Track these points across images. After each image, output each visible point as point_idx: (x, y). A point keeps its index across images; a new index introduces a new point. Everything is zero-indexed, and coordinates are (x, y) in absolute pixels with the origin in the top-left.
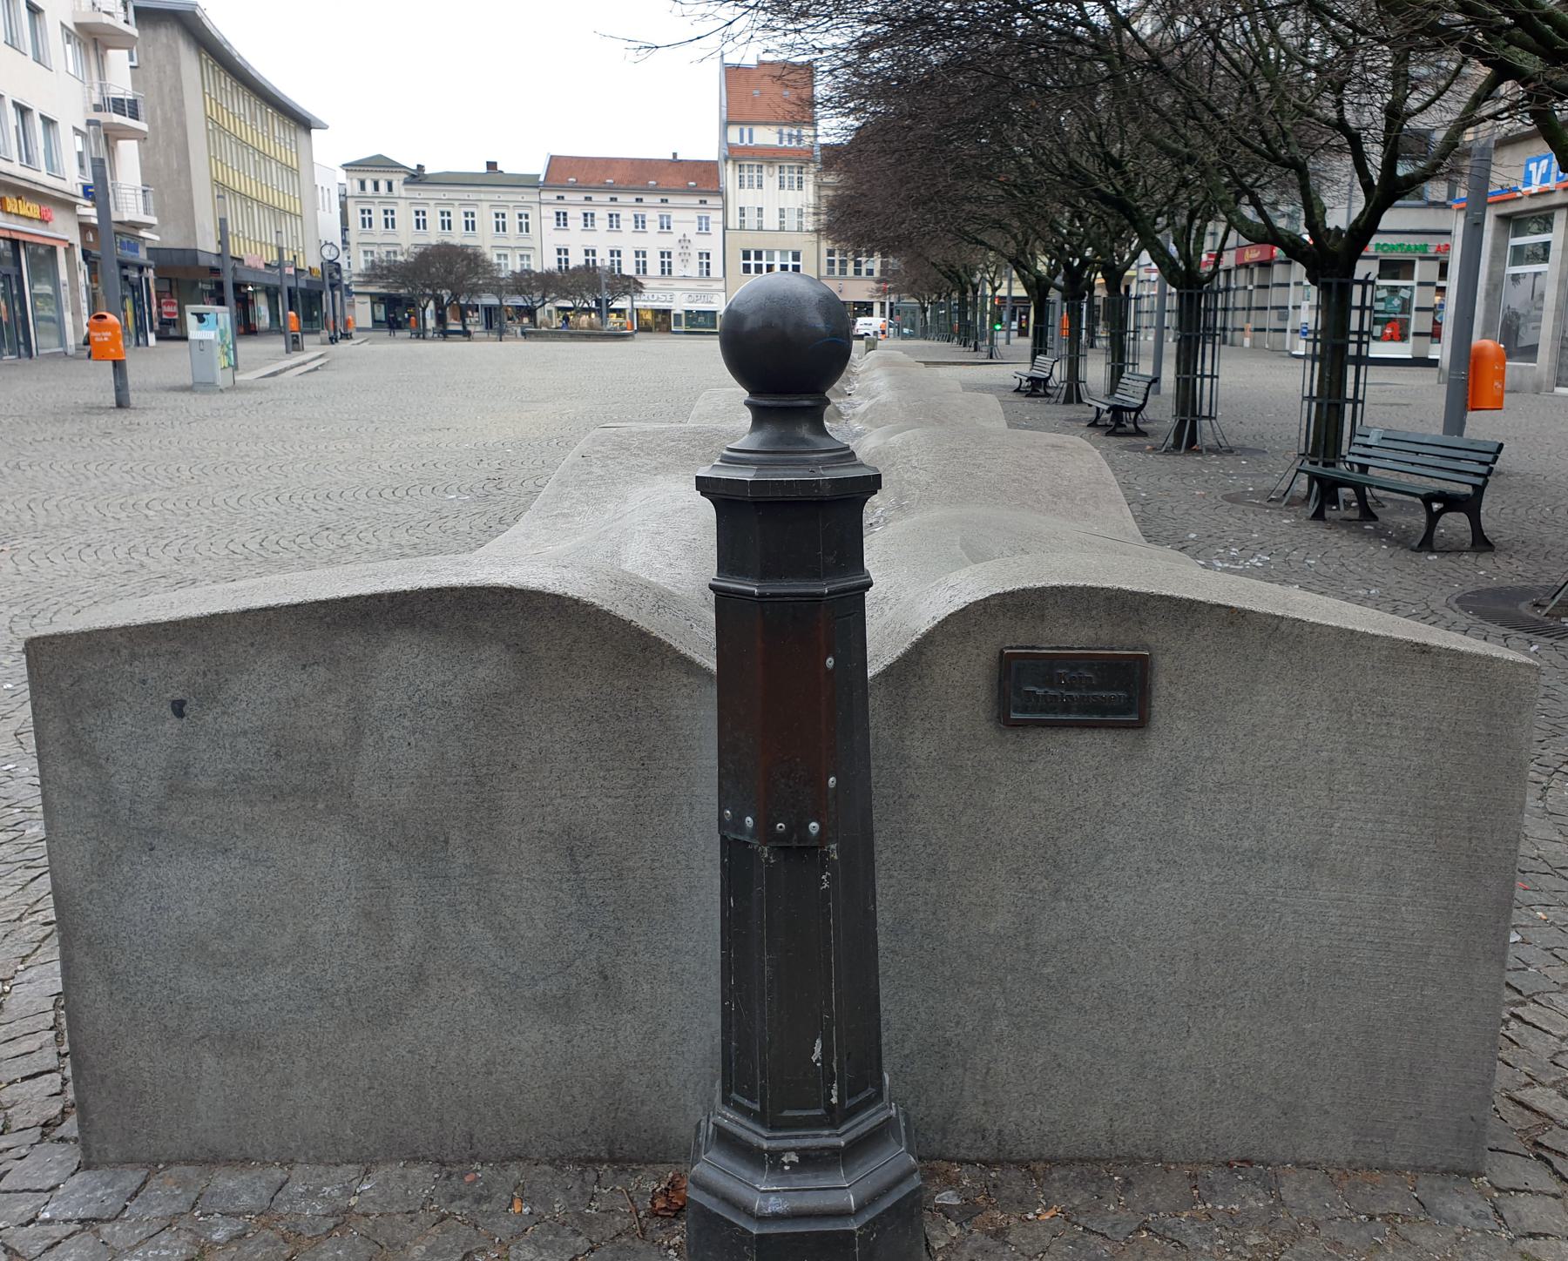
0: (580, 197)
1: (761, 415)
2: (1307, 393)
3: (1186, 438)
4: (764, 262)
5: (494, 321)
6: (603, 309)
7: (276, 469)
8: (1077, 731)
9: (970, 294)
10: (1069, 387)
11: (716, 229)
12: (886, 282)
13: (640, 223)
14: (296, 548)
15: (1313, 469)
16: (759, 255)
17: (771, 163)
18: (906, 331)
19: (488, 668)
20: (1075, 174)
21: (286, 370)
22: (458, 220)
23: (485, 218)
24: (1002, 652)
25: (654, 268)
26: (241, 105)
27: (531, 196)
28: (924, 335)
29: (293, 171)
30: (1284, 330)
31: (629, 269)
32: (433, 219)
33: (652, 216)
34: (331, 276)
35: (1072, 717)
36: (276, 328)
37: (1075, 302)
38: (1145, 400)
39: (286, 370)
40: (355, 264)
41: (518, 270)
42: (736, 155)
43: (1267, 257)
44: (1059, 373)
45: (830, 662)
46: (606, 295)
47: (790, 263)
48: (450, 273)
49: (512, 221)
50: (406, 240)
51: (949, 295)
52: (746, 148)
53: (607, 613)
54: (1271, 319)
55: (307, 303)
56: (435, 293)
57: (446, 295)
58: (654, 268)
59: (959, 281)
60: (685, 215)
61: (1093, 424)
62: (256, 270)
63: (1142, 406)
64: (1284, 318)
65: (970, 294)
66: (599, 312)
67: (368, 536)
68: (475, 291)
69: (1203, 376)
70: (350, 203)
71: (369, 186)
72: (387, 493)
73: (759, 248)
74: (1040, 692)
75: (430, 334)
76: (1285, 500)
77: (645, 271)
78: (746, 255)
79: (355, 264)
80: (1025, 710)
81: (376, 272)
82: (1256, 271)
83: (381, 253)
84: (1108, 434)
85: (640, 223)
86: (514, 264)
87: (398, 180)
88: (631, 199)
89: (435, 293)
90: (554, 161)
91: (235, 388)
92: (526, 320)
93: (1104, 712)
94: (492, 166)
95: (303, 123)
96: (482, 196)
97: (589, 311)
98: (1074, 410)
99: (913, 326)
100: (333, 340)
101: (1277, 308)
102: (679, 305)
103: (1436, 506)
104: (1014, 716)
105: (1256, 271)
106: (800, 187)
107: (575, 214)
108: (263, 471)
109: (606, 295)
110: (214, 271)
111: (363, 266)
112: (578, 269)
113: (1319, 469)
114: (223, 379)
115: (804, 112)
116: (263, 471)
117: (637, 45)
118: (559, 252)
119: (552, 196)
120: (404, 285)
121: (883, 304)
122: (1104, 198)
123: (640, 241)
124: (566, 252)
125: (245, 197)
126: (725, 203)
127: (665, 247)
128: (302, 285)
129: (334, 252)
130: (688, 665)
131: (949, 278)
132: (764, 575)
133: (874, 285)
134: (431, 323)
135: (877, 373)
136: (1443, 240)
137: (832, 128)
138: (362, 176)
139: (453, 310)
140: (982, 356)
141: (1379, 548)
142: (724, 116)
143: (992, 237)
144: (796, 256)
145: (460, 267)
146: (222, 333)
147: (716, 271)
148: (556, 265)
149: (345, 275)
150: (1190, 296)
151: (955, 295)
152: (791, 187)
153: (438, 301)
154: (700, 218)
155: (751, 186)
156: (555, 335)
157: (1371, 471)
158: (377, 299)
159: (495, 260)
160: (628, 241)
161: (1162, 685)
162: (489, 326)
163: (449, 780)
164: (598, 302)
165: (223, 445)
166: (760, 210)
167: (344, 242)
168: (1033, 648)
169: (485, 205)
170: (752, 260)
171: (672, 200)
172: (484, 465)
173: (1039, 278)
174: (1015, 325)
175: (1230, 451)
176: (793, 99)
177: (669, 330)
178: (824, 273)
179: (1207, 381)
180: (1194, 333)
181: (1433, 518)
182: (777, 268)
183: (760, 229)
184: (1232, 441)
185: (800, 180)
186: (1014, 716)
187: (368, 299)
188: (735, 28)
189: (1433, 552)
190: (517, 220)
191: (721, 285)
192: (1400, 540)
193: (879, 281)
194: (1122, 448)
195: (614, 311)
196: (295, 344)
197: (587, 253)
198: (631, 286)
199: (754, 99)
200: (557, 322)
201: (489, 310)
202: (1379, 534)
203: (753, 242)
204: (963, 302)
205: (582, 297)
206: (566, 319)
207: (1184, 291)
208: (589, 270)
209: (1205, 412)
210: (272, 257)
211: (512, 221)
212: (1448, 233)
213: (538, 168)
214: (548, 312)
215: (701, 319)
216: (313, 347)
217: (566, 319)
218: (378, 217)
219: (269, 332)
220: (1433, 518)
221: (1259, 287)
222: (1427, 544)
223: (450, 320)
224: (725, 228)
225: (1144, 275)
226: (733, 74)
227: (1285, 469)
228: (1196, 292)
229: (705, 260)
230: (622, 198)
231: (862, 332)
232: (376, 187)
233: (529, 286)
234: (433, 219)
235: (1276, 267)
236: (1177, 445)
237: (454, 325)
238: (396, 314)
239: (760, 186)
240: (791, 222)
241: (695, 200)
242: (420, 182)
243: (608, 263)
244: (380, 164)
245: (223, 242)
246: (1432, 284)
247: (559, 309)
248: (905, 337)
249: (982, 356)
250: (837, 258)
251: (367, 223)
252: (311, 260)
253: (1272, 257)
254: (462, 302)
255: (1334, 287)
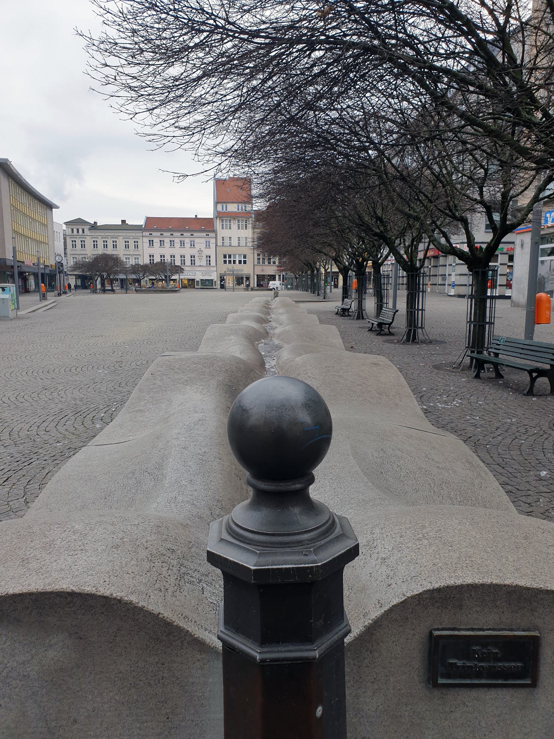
0: (158, 234)
1: (262, 498)
2: (469, 320)
3: (412, 335)
4: (232, 259)
5: (124, 284)
6: (167, 279)
7: (28, 358)
8: (486, 689)
9: (315, 272)
10: (359, 313)
11: (213, 246)
12: (281, 267)
13: (182, 244)
14: (31, 400)
15: (472, 355)
16: (230, 256)
17: (234, 219)
18: (289, 286)
19: (55, 651)
20: (362, 225)
21: (37, 310)
22: (110, 244)
23: (121, 243)
24: (431, 633)
25: (188, 262)
26: (25, 199)
27: (139, 234)
28: (297, 288)
29: (45, 226)
30: (445, 285)
31: (178, 263)
32: (100, 244)
33: (187, 241)
34: (59, 268)
35: (483, 681)
36: (38, 289)
37: (362, 276)
38: (393, 320)
39: (39, 309)
40: (69, 263)
41: (134, 264)
42: (219, 215)
43: (436, 254)
44: (354, 306)
45: (319, 711)
46: (169, 274)
47: (243, 259)
48: (107, 265)
49: (131, 244)
50: (90, 252)
51: (307, 272)
52: (224, 213)
53: (142, 609)
54: (440, 280)
55: (49, 280)
56: (101, 274)
57: (105, 275)
58: (188, 262)
59: (311, 266)
60: (200, 241)
61: (370, 330)
62: (29, 267)
63: (392, 323)
64: (444, 279)
65: (315, 272)
66: (166, 281)
67: (62, 393)
68: (116, 273)
69: (418, 310)
70: (68, 238)
71: (75, 231)
72: (73, 370)
73: (230, 253)
74: (460, 663)
75: (98, 291)
76: (458, 368)
77: (184, 264)
78: (225, 256)
79: (69, 263)
80: (448, 677)
81: (77, 266)
82: (432, 260)
83: (79, 258)
84: (377, 335)
85: (182, 244)
86: (132, 262)
87: (86, 228)
88: (179, 234)
89: (101, 274)
90: (148, 219)
91: (17, 318)
92: (137, 284)
93: (506, 678)
94: (124, 222)
95: (49, 206)
96: (120, 234)
97: (162, 280)
98: (361, 323)
99: (292, 285)
100: (59, 295)
101: (441, 275)
102: (198, 277)
103: (534, 375)
104: (441, 681)
105: (432, 260)
106: (246, 228)
107: (156, 241)
108: (23, 359)
109: (169, 274)
110: (12, 267)
111: (72, 263)
112: (157, 263)
113: (475, 355)
114: (12, 314)
115: (249, 199)
116: (23, 359)
117: (179, 175)
118: (150, 256)
119: (147, 234)
120: (88, 271)
121: (280, 276)
122: (376, 234)
123: (183, 251)
124: (153, 256)
125: (26, 237)
126: (216, 235)
127: (193, 254)
128: (47, 271)
129: (60, 258)
130: (201, 645)
131: (307, 265)
132: (265, 640)
133: (276, 268)
134: (99, 286)
135: (281, 310)
136: (511, 246)
137: (259, 205)
138: (72, 227)
139: (108, 281)
140: (321, 298)
141: (508, 394)
142: (216, 200)
143: (326, 250)
144: (245, 257)
145: (111, 263)
146: (12, 295)
147: (213, 263)
148: (149, 262)
149: (65, 267)
150: (412, 275)
151: (309, 272)
152: (242, 229)
153: (102, 277)
154: (206, 241)
155: (226, 228)
156: (148, 291)
157: (500, 356)
158: (78, 277)
159: (125, 260)
160: (177, 251)
161: (547, 656)
162: (122, 287)
163: (29, 730)
164: (166, 277)
165: (8, 346)
166: (230, 238)
167: (65, 253)
168: (454, 629)
169: (121, 238)
170: (227, 259)
171: (195, 234)
172: (115, 354)
173: (345, 267)
174: (333, 283)
175: (431, 342)
176: (245, 194)
177: (194, 287)
178: (256, 263)
179: (420, 312)
180: (414, 291)
181: (533, 380)
182: (237, 262)
183: (230, 246)
184: (431, 337)
185: (246, 227)
186: (441, 681)
187: (74, 277)
188: (223, 166)
189: (534, 395)
190: (134, 244)
191: (215, 269)
192: (517, 389)
193: (278, 267)
194: (385, 341)
195: (172, 280)
196: (44, 297)
197: (161, 256)
198: (179, 270)
199: (227, 193)
200: (149, 285)
201: (122, 280)
202: (506, 386)
203: (227, 251)
204: (312, 275)
205: (159, 274)
206: (153, 284)
207: (410, 274)
208: (162, 264)
209: (420, 325)
210: (36, 261)
211: (131, 244)
212: (513, 243)
213: (142, 222)
214: (145, 282)
215: (207, 283)
216: (51, 297)
217: (153, 284)
218: (78, 244)
219: (34, 291)
220: (533, 380)
221: (434, 266)
222: (530, 393)
223: (106, 285)
224: (216, 245)
225: (389, 266)
226: (220, 184)
227: (459, 352)
228: (415, 273)
229: (208, 259)
230: (175, 234)
231: (271, 288)
232: (78, 231)
233: (138, 270)
234: (100, 244)
235: (441, 258)
236: (408, 340)
237: (108, 287)
238: (85, 283)
239: (230, 228)
240: (243, 243)
241: (204, 234)
242: (95, 229)
243: (169, 261)
244: (79, 222)
245: (14, 256)
246: (506, 264)
247: (150, 279)
248: (289, 289)
249: (321, 298)
250: (261, 257)
251: (74, 246)
252: (52, 262)
253: (439, 254)
254: (111, 277)
255: (480, 273)
